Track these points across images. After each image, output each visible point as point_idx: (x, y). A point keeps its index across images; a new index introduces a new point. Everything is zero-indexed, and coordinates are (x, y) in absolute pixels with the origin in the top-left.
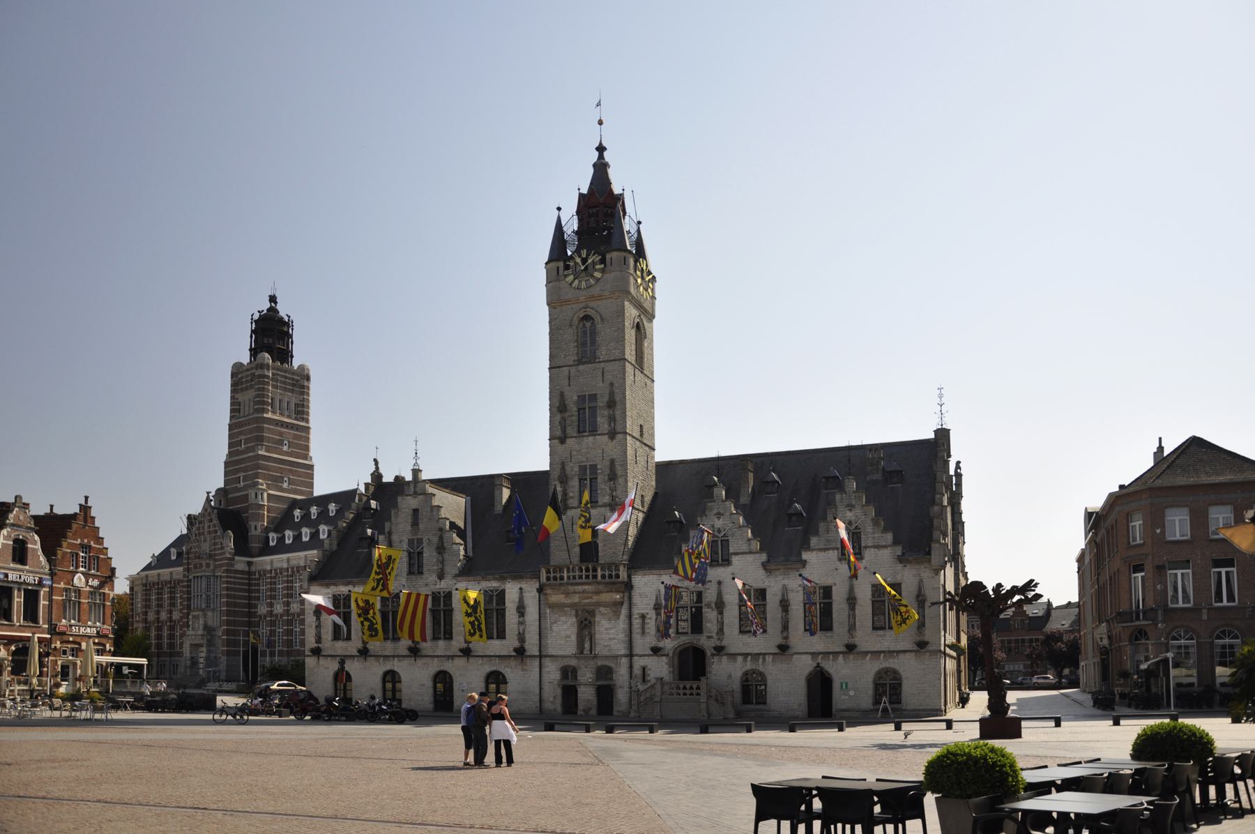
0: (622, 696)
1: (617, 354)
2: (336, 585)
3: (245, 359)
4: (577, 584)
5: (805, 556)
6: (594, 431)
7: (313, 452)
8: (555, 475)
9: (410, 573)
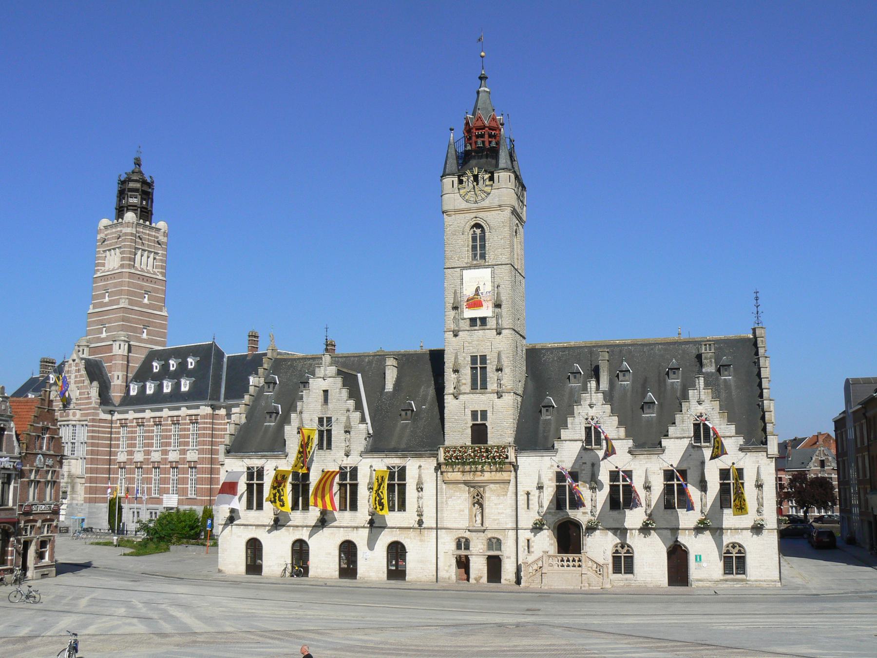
2: (249, 457)
5: (665, 442)
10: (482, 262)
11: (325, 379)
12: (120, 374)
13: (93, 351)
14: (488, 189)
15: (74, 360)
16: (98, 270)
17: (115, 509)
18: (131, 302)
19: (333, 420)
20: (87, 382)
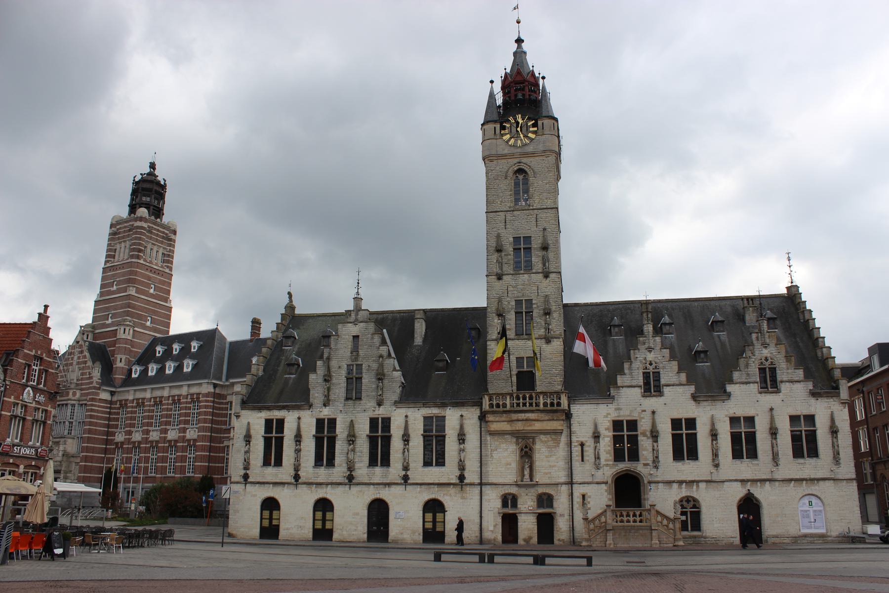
0: (562, 525)
1: (549, 203)
3: (124, 213)
4: (532, 411)
5: (729, 388)
6: (529, 268)
7: (172, 296)
8: (493, 308)
9: (348, 399)
17: (109, 480)
20: (90, 363)
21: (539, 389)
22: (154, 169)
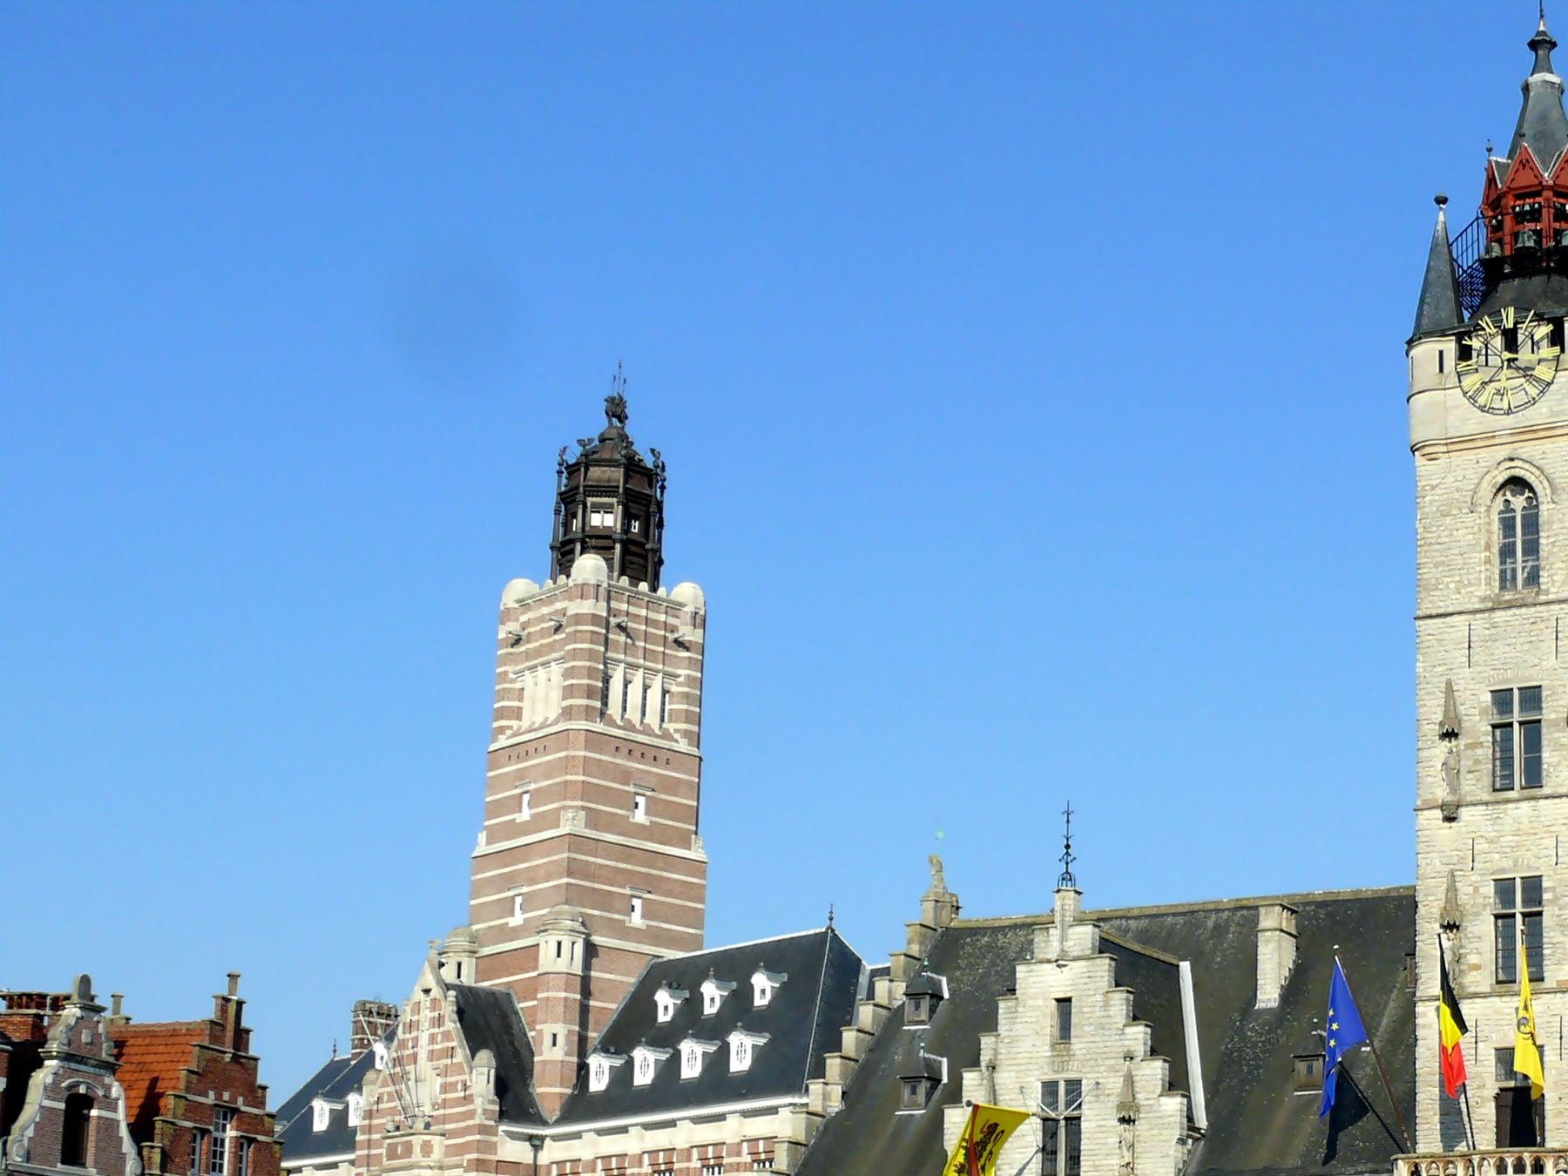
10: (1529, 594)
11: (1063, 973)
12: (561, 1030)
13: (487, 966)
14: (1544, 372)
15: (427, 991)
16: (502, 730)
18: (594, 819)
19: (1086, 1087)
20: (461, 1054)
21: (1549, 1144)
22: (622, 418)
